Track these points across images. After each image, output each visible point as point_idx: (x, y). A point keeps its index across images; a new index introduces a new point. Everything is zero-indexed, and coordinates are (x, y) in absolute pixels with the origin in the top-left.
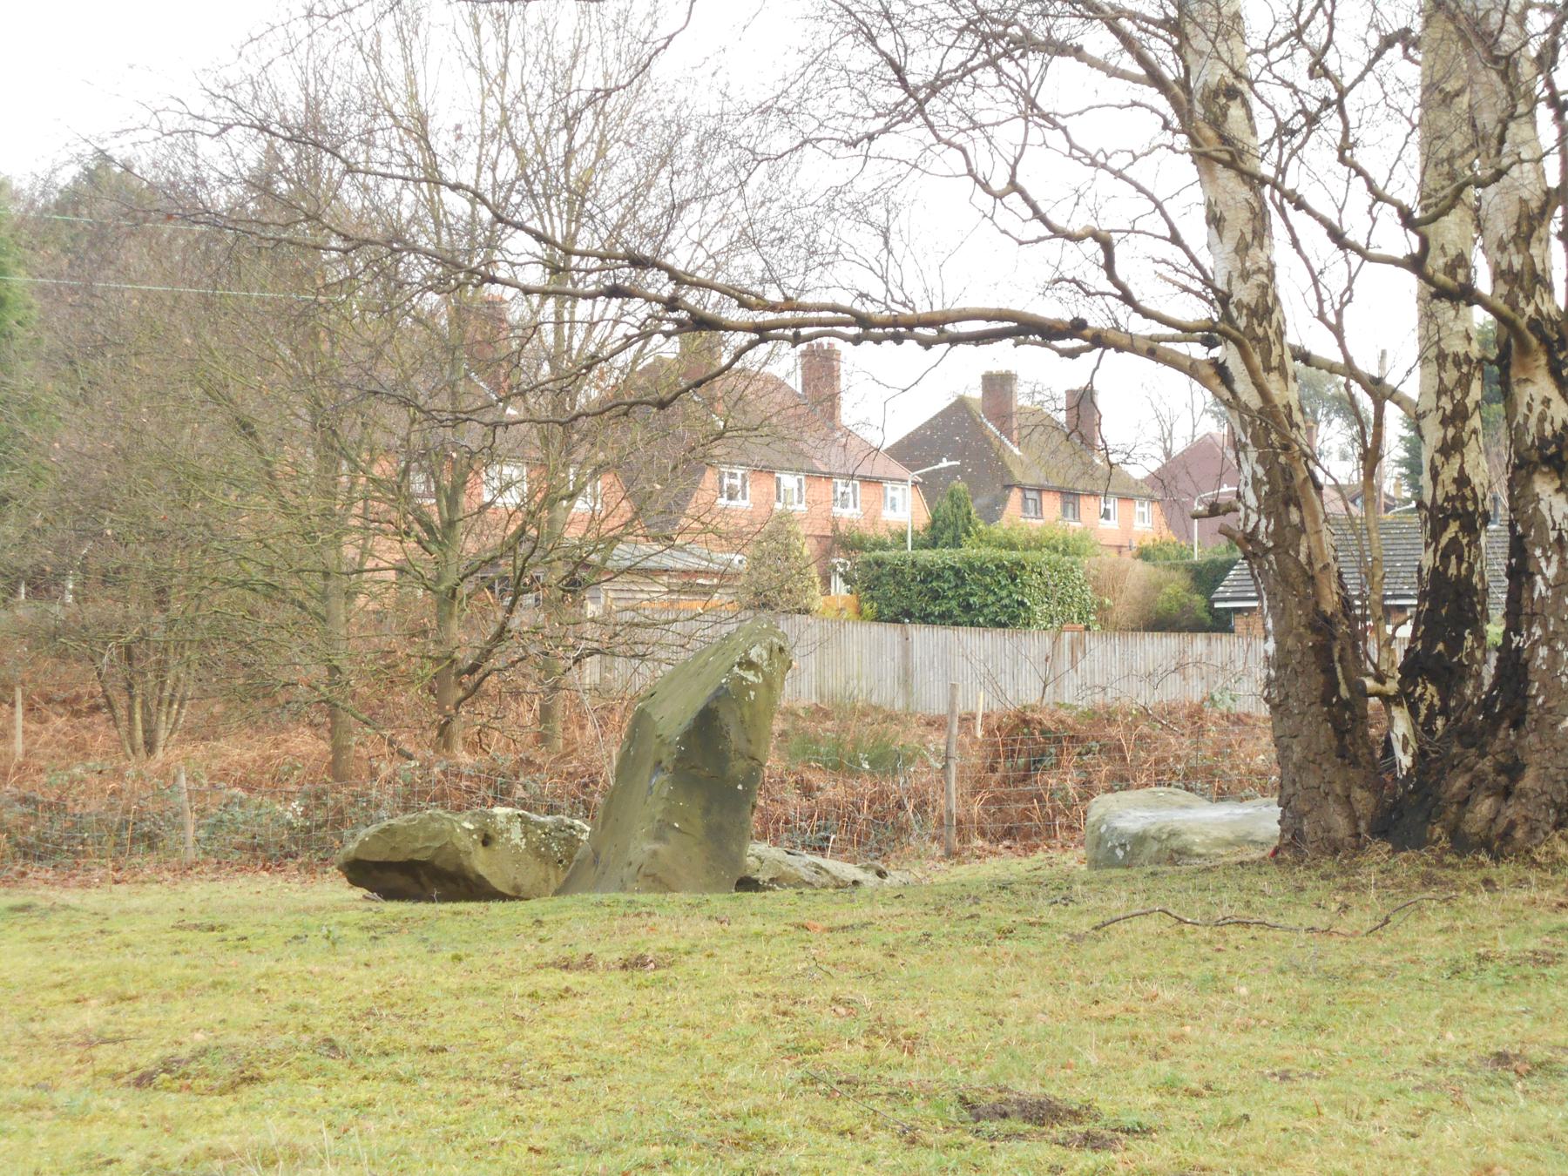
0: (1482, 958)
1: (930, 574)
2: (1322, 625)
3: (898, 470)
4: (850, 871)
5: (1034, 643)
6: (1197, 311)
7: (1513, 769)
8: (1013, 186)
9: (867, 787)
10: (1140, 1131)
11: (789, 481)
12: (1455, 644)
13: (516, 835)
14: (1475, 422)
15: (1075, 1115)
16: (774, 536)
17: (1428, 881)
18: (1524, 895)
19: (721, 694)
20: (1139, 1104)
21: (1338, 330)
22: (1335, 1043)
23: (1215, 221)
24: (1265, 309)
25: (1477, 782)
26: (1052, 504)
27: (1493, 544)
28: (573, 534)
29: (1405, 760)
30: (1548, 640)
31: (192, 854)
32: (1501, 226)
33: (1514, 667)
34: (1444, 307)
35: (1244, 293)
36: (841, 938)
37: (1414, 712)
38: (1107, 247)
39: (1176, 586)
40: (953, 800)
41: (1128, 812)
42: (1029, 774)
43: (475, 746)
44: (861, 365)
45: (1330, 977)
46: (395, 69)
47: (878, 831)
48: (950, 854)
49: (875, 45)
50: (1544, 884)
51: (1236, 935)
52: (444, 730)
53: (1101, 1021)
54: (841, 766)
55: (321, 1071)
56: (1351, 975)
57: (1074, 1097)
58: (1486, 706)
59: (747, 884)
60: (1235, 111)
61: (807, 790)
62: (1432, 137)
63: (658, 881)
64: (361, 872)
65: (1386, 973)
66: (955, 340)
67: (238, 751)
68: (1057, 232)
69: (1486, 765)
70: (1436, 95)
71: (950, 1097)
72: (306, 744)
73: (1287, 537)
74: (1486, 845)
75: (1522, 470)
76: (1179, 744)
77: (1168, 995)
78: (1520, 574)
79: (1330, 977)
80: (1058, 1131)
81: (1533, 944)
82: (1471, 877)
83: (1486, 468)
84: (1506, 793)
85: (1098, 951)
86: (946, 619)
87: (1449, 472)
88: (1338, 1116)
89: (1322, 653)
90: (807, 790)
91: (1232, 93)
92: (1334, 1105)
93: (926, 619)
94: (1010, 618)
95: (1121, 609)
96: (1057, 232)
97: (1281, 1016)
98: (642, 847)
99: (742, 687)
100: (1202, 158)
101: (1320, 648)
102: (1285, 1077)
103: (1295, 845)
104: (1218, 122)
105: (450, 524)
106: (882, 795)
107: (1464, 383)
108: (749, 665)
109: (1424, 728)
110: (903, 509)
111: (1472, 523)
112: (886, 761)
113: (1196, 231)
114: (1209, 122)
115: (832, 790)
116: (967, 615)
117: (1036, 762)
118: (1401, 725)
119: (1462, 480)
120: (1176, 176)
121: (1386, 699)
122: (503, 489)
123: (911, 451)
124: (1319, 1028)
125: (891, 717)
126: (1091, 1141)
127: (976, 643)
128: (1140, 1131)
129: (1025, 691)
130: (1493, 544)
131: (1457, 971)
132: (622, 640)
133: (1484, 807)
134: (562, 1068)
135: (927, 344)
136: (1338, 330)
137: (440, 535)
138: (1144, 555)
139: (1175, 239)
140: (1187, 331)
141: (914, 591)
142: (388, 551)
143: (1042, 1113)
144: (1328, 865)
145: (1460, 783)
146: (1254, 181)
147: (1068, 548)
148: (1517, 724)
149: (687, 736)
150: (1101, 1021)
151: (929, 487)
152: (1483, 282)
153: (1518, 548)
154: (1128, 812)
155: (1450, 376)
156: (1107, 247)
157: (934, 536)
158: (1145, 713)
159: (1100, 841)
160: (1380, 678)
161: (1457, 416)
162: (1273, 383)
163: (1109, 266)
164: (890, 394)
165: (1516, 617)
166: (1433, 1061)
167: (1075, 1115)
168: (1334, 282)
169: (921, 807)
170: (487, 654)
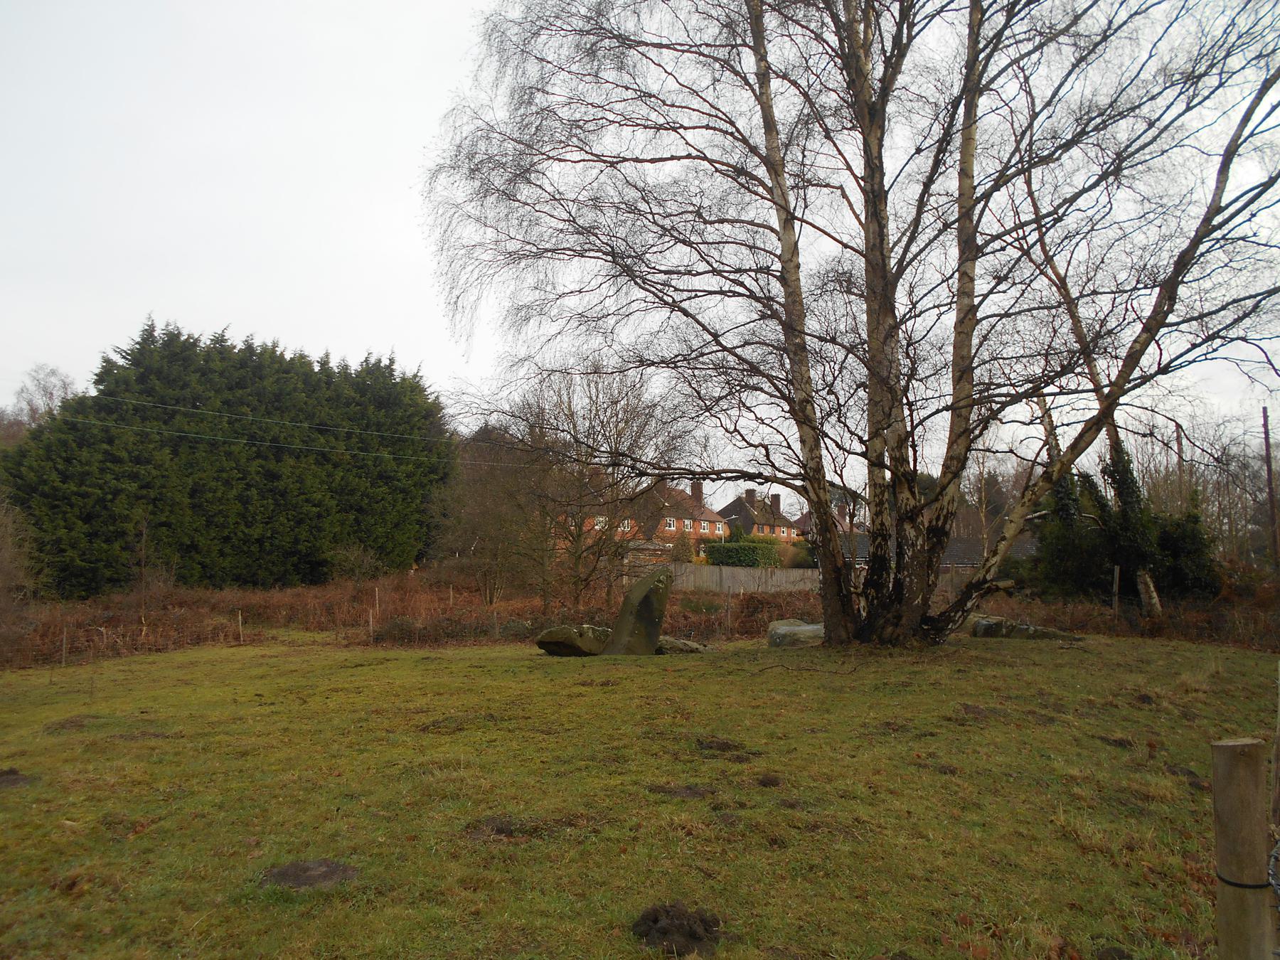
0: (885, 684)
1: (729, 550)
2: (837, 571)
3: (719, 518)
4: (695, 645)
5: (757, 572)
6: (795, 469)
7: (899, 617)
8: (736, 430)
9: (704, 618)
10: (757, 754)
11: (687, 522)
12: (880, 577)
13: (590, 634)
14: (886, 505)
15: (736, 748)
16: (681, 538)
17: (871, 654)
18: (902, 659)
19: (654, 591)
20: (759, 742)
21: (841, 476)
22: (832, 717)
23: (803, 441)
24: (819, 469)
25: (887, 621)
26: (767, 529)
27: (892, 544)
28: (617, 538)
29: (864, 614)
30: (909, 576)
31: (498, 637)
32: (892, 443)
33: (898, 583)
34: (876, 470)
35: (812, 464)
36: (676, 674)
37: (867, 598)
38: (767, 450)
39: (803, 554)
40: (729, 622)
41: (781, 628)
42: (754, 612)
43: (587, 604)
44: (707, 486)
45: (834, 690)
46: (565, 398)
47: (706, 632)
48: (729, 639)
49: (560, 371)
50: (909, 655)
51: (805, 674)
52: (577, 599)
53: (753, 707)
54: (696, 610)
55: (484, 726)
56: (841, 690)
57: (733, 738)
58: (890, 597)
59: (660, 651)
60: (809, 407)
61: (686, 618)
62: (871, 416)
63: (630, 650)
64: (541, 644)
65: (853, 689)
66: (723, 478)
67: (517, 604)
68: (751, 445)
69: (890, 616)
70: (872, 402)
71: (694, 739)
72: (537, 602)
73: (826, 542)
74: (890, 642)
75: (900, 521)
76: (800, 604)
77: (778, 698)
78: (900, 555)
79: (834, 690)
80: (728, 754)
81: (903, 678)
82: (885, 652)
83: (888, 520)
84: (896, 625)
85: (759, 680)
86: (734, 565)
87: (878, 521)
88: (828, 749)
89: (838, 580)
90: (686, 618)
91: (808, 402)
92: (826, 744)
93: (727, 564)
94: (752, 564)
95: (786, 560)
96: (751, 445)
97: (815, 706)
98: (626, 639)
99: (657, 588)
100: (799, 423)
101: (837, 576)
102: (813, 731)
103: (829, 641)
104: (803, 410)
105: (579, 536)
106: (708, 620)
107: (882, 493)
108: (660, 581)
109: (870, 604)
110: (721, 530)
111: (885, 538)
112: (712, 608)
113: (797, 446)
114: (801, 412)
115: (693, 618)
116: (739, 563)
117: (756, 609)
118: (863, 603)
119: (882, 524)
120: (792, 430)
121: (858, 595)
122: (600, 523)
123: (724, 513)
124: (828, 711)
125: (715, 594)
126: (740, 760)
127: (741, 572)
128: (757, 754)
129: (753, 588)
130: (892, 544)
131: (877, 688)
132: (633, 571)
133: (890, 629)
134: (567, 726)
135: (713, 480)
136: (841, 476)
137: (577, 538)
138: (794, 544)
139: (789, 447)
140: (795, 477)
141: (721, 555)
142: (562, 544)
143: (725, 747)
144: (840, 648)
145: (882, 622)
146: (814, 428)
147: (771, 542)
148: (900, 603)
149: (641, 604)
150: (753, 707)
151: (730, 524)
152: (887, 461)
153: (899, 546)
154: (781, 628)
155: (878, 491)
156: (767, 450)
157: (730, 539)
158: (790, 594)
159: (772, 637)
160: (856, 588)
161: (881, 503)
162: (821, 493)
163: (767, 456)
164: (719, 496)
165: (899, 568)
166: (864, 725)
167: (736, 748)
168: (840, 460)
169: (720, 624)
170: (590, 575)
